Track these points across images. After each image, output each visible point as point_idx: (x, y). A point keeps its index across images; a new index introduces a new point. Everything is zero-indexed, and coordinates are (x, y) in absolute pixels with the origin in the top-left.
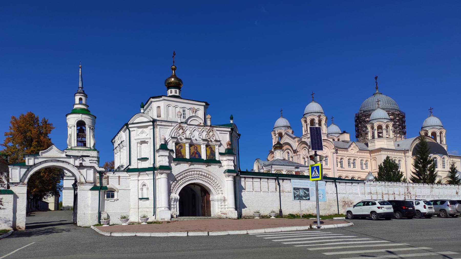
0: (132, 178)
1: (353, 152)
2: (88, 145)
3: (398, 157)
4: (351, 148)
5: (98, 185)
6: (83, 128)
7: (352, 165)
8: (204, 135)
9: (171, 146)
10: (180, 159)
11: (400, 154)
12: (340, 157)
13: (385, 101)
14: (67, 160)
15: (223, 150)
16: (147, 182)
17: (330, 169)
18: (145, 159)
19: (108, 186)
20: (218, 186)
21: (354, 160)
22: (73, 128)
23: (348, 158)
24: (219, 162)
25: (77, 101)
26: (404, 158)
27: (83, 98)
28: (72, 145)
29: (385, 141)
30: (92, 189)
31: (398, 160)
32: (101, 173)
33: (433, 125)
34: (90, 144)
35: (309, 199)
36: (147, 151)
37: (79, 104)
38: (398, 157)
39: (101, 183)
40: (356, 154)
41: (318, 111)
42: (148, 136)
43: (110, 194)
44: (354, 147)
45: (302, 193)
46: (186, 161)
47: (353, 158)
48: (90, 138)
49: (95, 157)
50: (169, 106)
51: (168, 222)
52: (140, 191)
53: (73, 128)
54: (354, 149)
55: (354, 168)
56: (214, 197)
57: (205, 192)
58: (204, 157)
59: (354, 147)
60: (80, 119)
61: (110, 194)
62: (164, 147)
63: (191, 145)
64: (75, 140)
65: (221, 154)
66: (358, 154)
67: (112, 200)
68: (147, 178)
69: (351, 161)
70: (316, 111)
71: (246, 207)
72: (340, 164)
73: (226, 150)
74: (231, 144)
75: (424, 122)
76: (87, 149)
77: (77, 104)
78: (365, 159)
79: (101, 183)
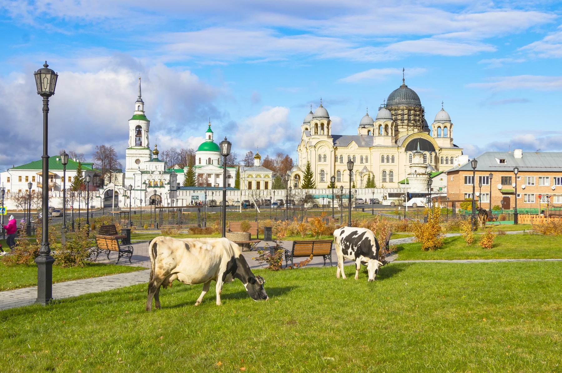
2: (143, 145)
6: (141, 129)
13: (402, 96)
15: (166, 183)
22: (133, 131)
25: (137, 109)
27: (141, 105)
30: (123, 196)
32: (125, 191)
33: (439, 120)
34: (145, 144)
37: (138, 111)
39: (125, 194)
41: (321, 116)
45: (195, 197)
46: (152, 187)
48: (145, 139)
58: (159, 186)
62: (144, 183)
66: (358, 150)
70: (319, 116)
71: (366, 187)
73: (168, 183)
74: (170, 181)
79: (125, 194)
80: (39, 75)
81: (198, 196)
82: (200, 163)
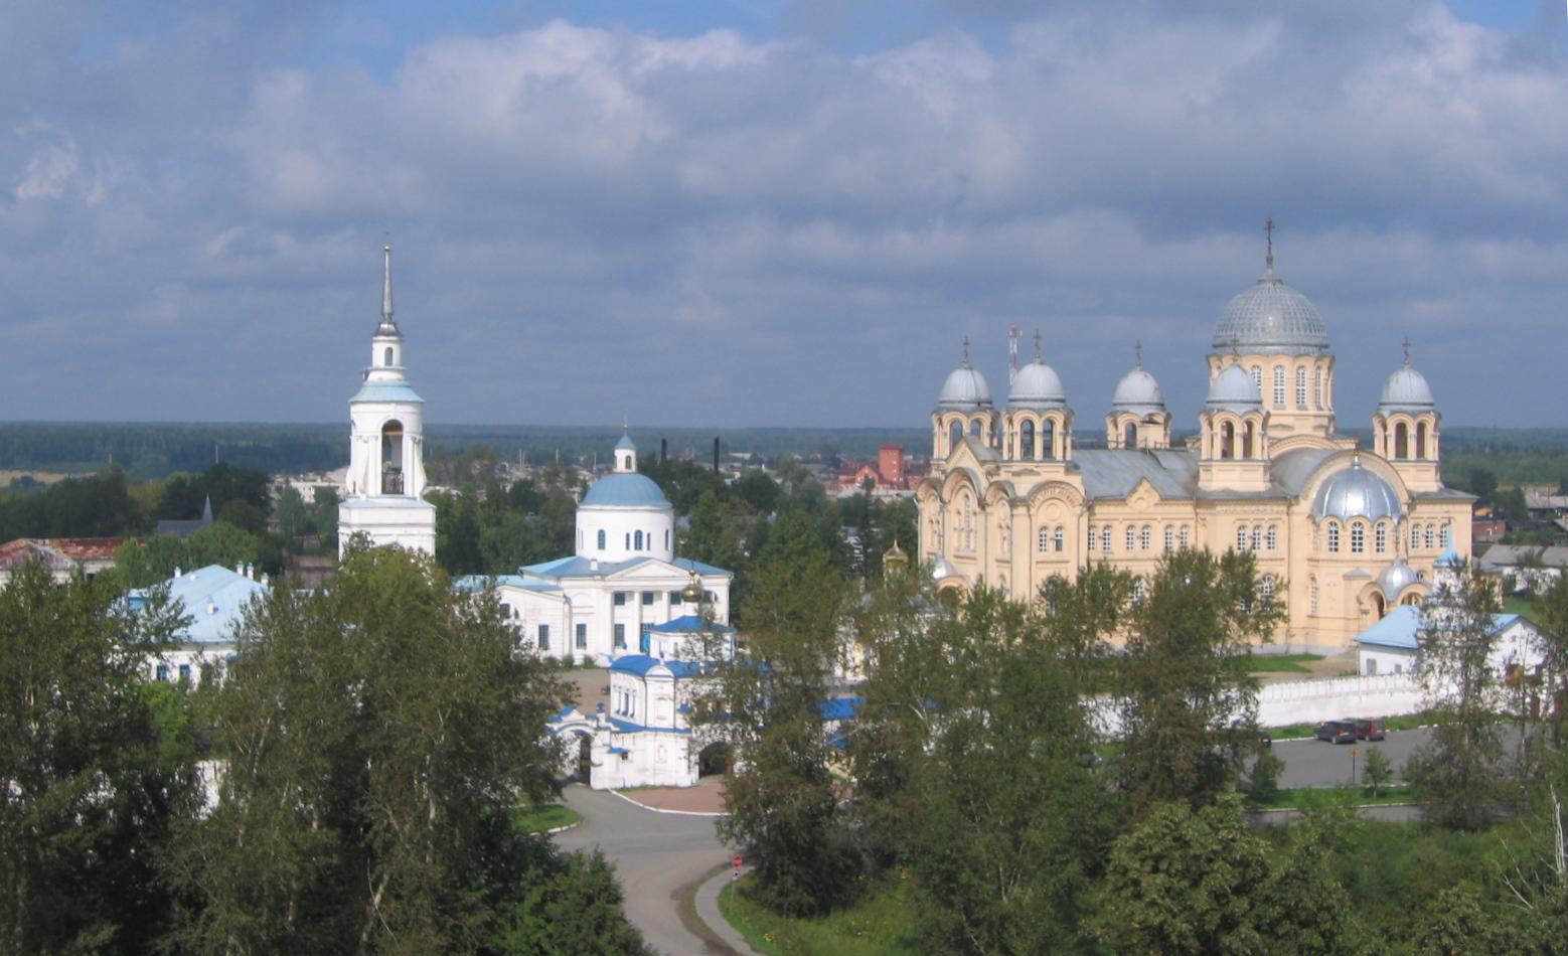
1: (1142, 505)
3: (1252, 517)
4: (1136, 496)
7: (1138, 543)
11: (1275, 508)
12: (1101, 524)
17: (1067, 562)
18: (601, 545)
21: (1107, 527)
23: (1127, 523)
26: (1285, 518)
29: (1239, 470)
31: (1267, 525)
38: (1425, 516)
40: (1152, 510)
43: (624, 755)
44: (1146, 491)
47: (1140, 524)
49: (309, 570)
54: (1145, 496)
55: (1380, 553)
59: (1146, 491)
64: (376, 476)
66: (1160, 509)
69: (1138, 531)
72: (1438, 539)
75: (445, 544)
77: (377, 369)
78: (1178, 524)
80: (964, 534)
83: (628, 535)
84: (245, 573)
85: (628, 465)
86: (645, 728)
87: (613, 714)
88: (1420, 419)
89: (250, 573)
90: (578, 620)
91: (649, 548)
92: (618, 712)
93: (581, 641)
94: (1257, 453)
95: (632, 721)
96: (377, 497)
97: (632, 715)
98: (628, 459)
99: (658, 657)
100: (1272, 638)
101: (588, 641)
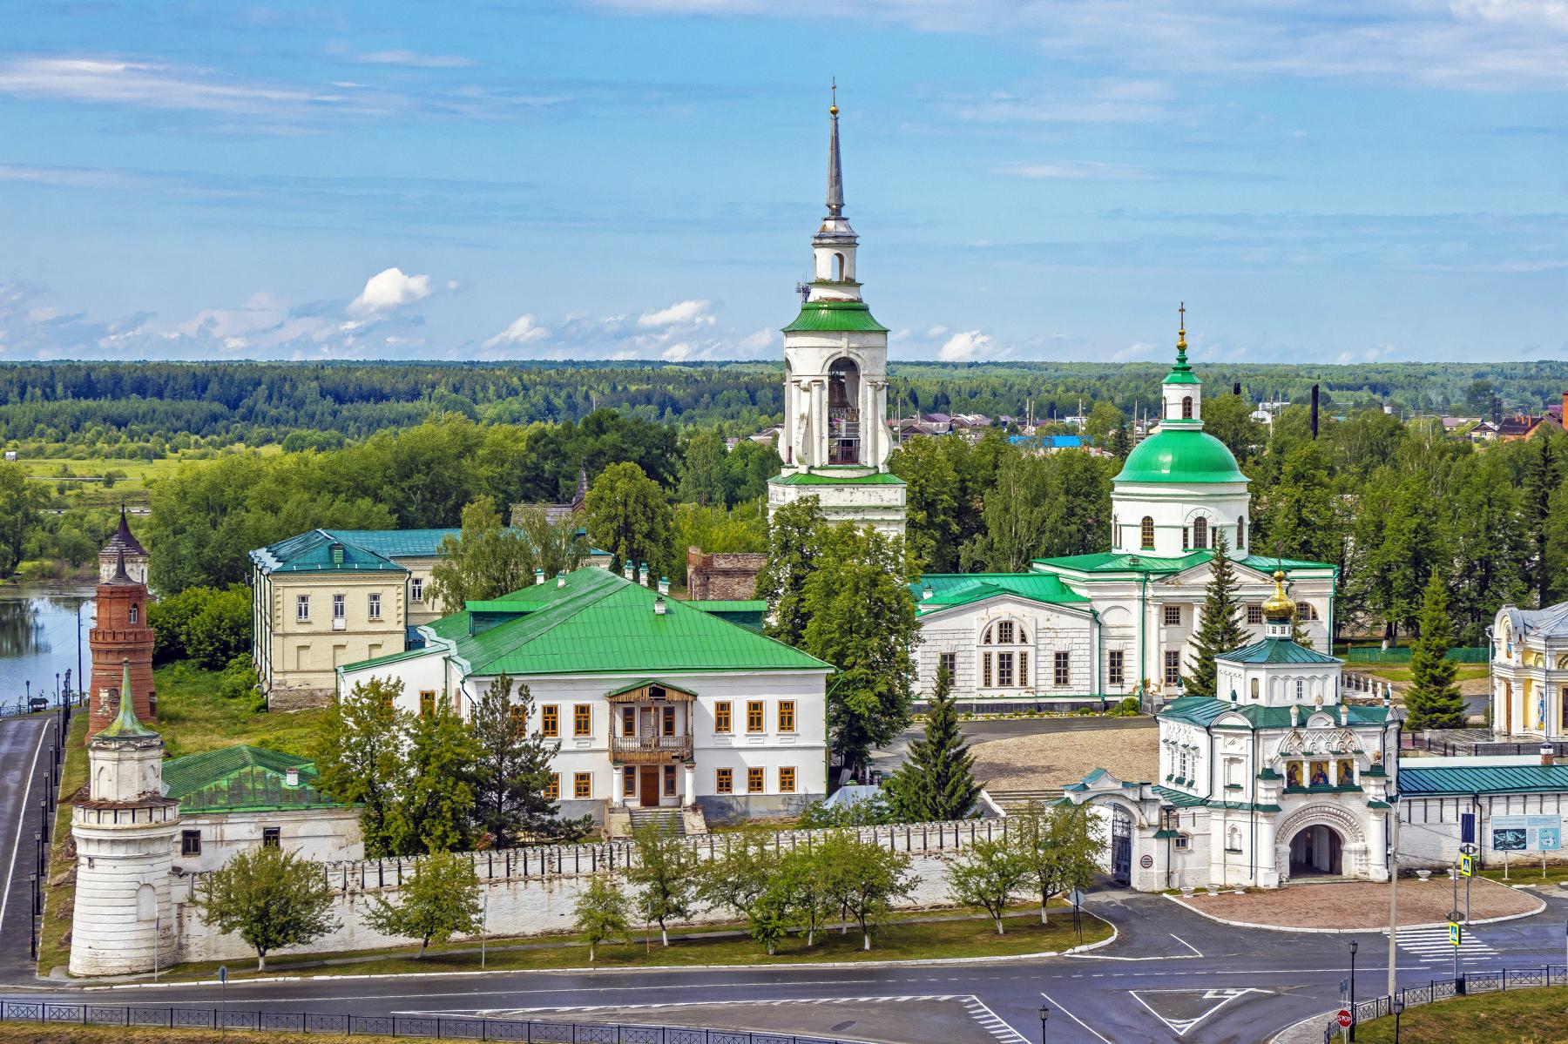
0: (1214, 816)
2: (866, 458)
5: (1165, 828)
8: (1335, 746)
9: (1282, 769)
10: (1294, 787)
14: (1125, 793)
16: (1239, 825)
19: (1178, 830)
20: (1359, 834)
22: (815, 390)
24: (1359, 789)
28: (812, 458)
30: (1155, 837)
35: (1524, 848)
36: (1241, 775)
42: (1243, 752)
43: (1182, 841)
45: (1510, 838)
46: (1302, 790)
50: (1274, 679)
51: (1275, 890)
52: (1228, 839)
53: (815, 390)
56: (1350, 845)
57: (1335, 840)
58: (1333, 780)
60: (843, 355)
61: (1182, 841)
63: (1312, 764)
65: (1362, 774)
67: (1184, 850)
68: (1241, 821)
76: (863, 473)
81: (1523, 832)
82: (1148, 542)
83: (1241, 519)
84: (636, 578)
85: (1187, 413)
86: (1204, 802)
87: (1163, 782)
88: (339, 623)
89: (644, 577)
90: (1113, 645)
91: (1023, 682)
92: (1170, 778)
93: (1116, 677)
94: (877, 445)
95: (1191, 792)
96: (822, 468)
97: (1191, 784)
98: (1187, 402)
99: (1229, 700)
100: (740, 476)
101: (1125, 676)
